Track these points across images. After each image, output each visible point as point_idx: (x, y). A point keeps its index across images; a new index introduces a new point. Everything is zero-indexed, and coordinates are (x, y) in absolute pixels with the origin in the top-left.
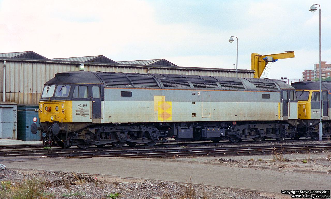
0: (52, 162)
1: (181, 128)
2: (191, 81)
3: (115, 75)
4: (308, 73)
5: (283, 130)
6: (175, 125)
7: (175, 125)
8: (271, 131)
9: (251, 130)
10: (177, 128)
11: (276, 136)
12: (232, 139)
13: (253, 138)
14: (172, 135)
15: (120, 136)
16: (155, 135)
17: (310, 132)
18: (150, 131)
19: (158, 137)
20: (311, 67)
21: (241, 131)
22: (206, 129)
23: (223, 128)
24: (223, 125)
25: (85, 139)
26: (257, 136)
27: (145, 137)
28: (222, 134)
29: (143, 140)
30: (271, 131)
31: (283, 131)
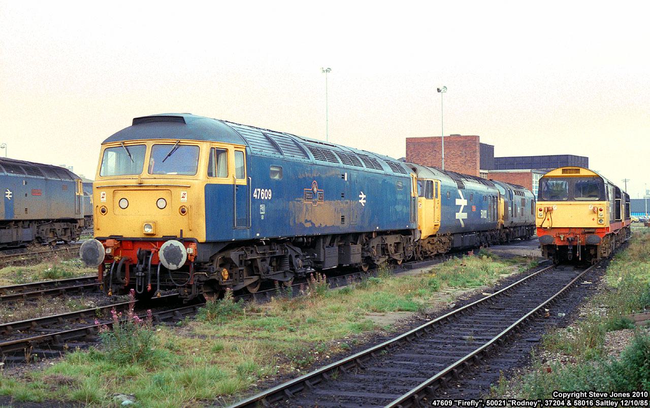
6: (322, 240)
7: (322, 240)
12: (206, 293)
26: (255, 278)
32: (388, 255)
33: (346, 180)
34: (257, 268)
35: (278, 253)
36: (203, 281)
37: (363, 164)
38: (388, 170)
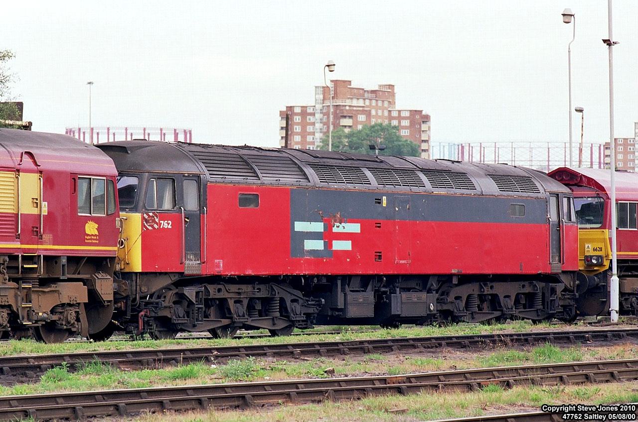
0: (588, 344)
1: (351, 291)
2: (366, 168)
3: (209, 150)
4: (297, 114)
5: (551, 299)
6: (339, 282)
7: (339, 282)
8: (258, 306)
9: (208, 303)
10: (343, 290)
11: (271, 322)
13: (212, 329)
14: (330, 308)
15: (292, 309)
16: (298, 307)
17: (148, 317)
18: (288, 299)
19: (302, 314)
20: (306, 96)
21: (513, 298)
22: (400, 293)
23: (432, 293)
24: (432, 285)
25: (455, 311)
26: (226, 322)
27: (278, 314)
28: (432, 309)
29: (537, 312)
30: (258, 306)
31: (552, 300)
32: (502, 311)
33: (384, 205)
34: (229, 310)
35: (264, 294)
36: (151, 317)
37: (368, 174)
38: (489, 187)
